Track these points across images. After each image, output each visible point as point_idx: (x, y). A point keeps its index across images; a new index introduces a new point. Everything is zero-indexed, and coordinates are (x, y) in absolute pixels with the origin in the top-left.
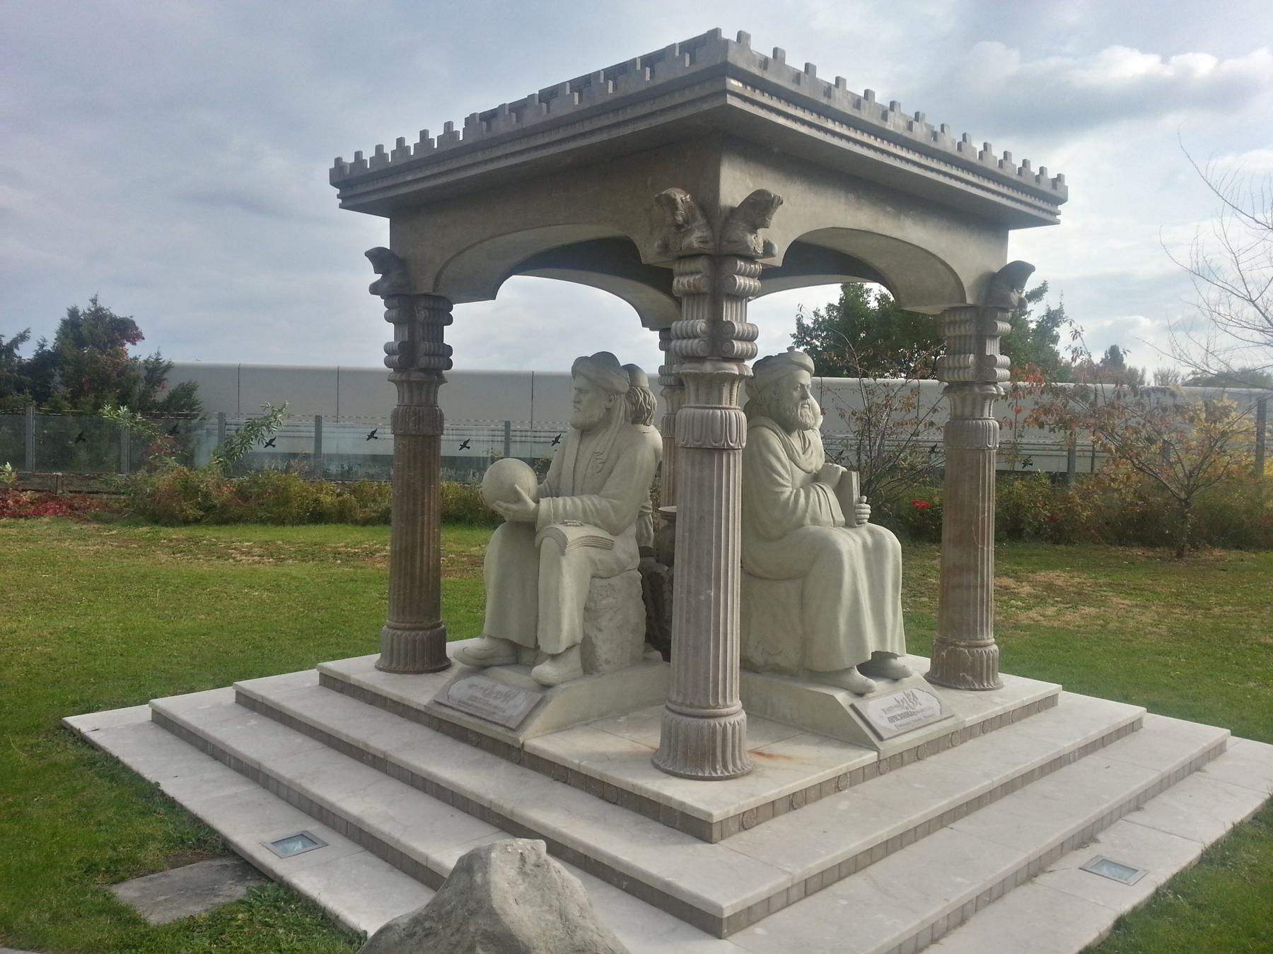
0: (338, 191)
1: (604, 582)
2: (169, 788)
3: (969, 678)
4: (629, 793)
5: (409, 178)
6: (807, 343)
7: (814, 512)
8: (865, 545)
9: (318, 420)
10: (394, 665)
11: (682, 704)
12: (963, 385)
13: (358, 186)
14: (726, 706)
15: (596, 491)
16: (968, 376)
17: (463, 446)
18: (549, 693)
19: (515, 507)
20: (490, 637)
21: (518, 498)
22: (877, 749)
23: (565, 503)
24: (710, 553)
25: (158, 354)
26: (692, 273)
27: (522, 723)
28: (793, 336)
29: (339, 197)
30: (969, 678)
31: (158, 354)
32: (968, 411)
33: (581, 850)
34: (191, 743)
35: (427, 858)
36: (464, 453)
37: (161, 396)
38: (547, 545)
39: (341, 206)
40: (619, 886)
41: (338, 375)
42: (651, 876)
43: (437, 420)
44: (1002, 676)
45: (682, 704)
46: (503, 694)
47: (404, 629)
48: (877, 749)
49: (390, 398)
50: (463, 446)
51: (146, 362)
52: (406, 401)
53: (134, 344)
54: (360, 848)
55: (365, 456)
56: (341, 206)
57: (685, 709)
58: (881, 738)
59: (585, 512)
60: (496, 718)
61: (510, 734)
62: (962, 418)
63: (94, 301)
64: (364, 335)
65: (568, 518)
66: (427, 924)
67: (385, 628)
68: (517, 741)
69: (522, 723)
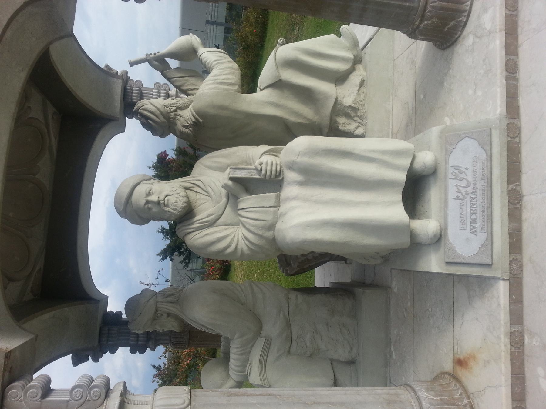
1: (294, 344)
3: (452, 24)
7: (263, 228)
8: (301, 184)
25: (173, 150)
30: (452, 24)
31: (173, 150)
37: (190, 151)
51: (176, 155)
53: (168, 155)
63: (150, 168)
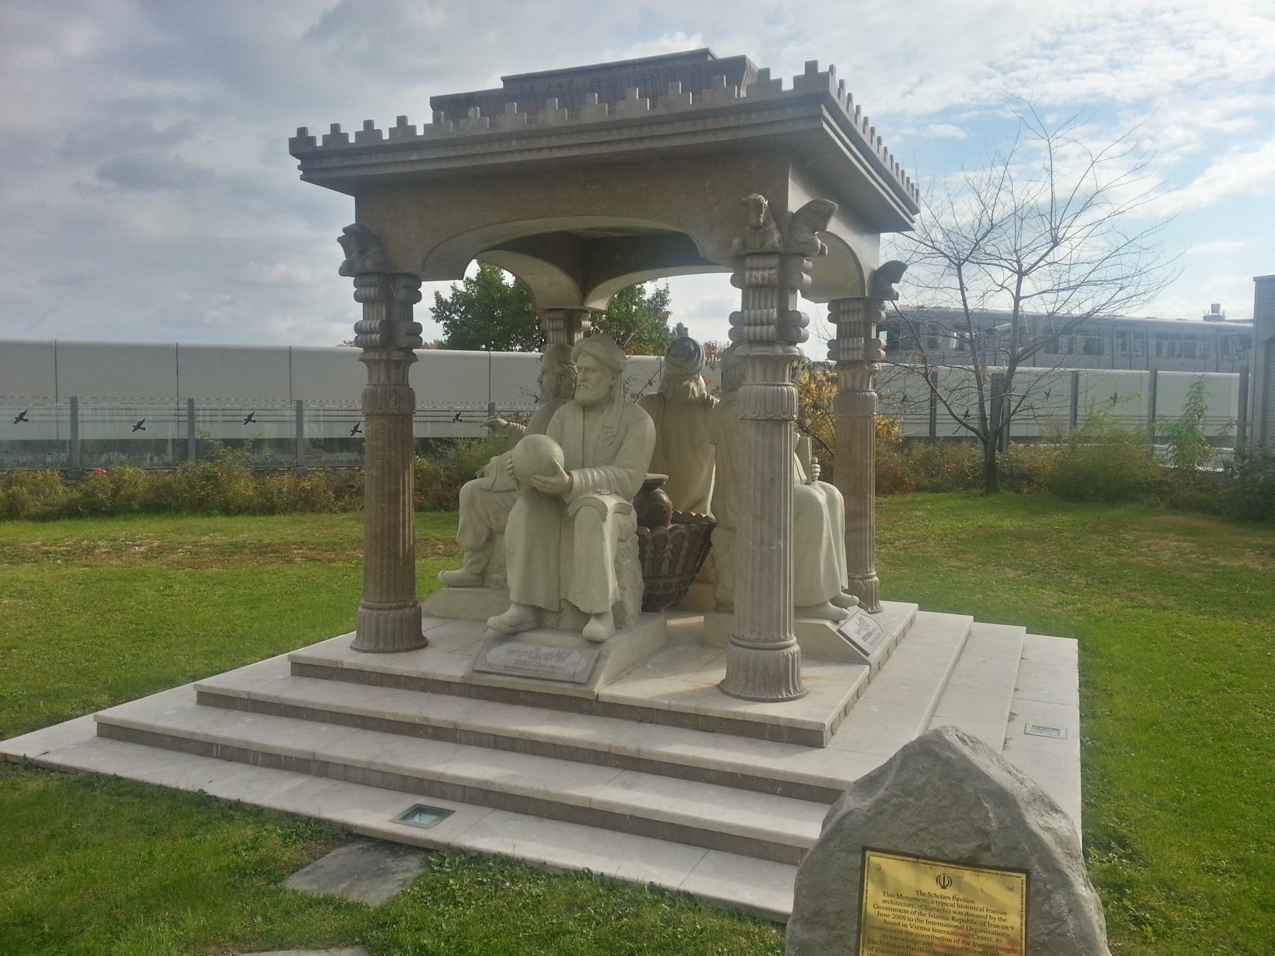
0: (298, 162)
2: (212, 790)
4: (728, 720)
5: (414, 158)
6: (447, 318)
9: (74, 401)
10: (382, 646)
11: (758, 640)
12: (854, 363)
13: (321, 160)
14: (781, 640)
15: (610, 461)
16: (859, 356)
17: (136, 428)
18: (602, 648)
19: (553, 480)
20: (519, 604)
21: (554, 469)
22: (867, 663)
23: (593, 475)
24: (779, 509)
26: (764, 269)
27: (590, 677)
28: (432, 310)
29: (299, 168)
32: (857, 385)
33: (728, 770)
34: (190, 751)
35: (590, 800)
36: (139, 435)
38: (584, 516)
39: (302, 178)
40: (773, 793)
41: (291, 357)
42: (812, 777)
43: (408, 397)
44: (882, 603)
45: (758, 640)
46: (551, 654)
47: (390, 609)
48: (867, 663)
49: (359, 380)
50: (136, 428)
52: (383, 380)
53: (804, 340)
54: (488, 810)
55: (13, 442)
56: (302, 178)
57: (761, 644)
58: (867, 655)
59: (608, 482)
60: (559, 676)
61: (582, 688)
62: (853, 390)
64: (330, 314)
65: (596, 488)
66: (894, 801)
67: (360, 609)
68: (592, 693)
69: (590, 677)
